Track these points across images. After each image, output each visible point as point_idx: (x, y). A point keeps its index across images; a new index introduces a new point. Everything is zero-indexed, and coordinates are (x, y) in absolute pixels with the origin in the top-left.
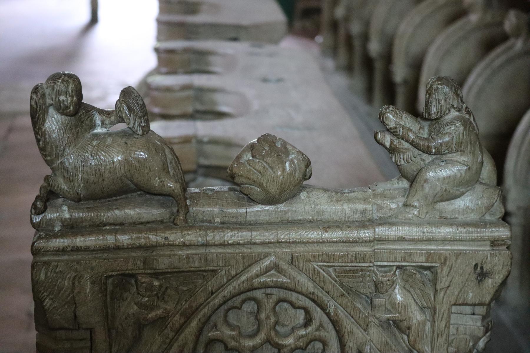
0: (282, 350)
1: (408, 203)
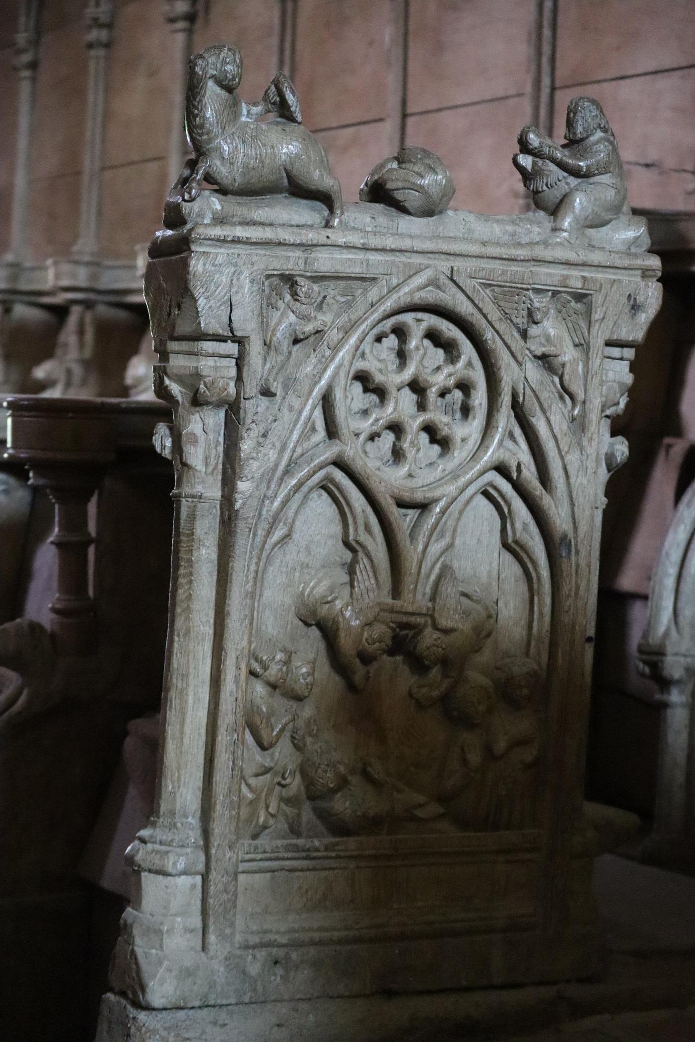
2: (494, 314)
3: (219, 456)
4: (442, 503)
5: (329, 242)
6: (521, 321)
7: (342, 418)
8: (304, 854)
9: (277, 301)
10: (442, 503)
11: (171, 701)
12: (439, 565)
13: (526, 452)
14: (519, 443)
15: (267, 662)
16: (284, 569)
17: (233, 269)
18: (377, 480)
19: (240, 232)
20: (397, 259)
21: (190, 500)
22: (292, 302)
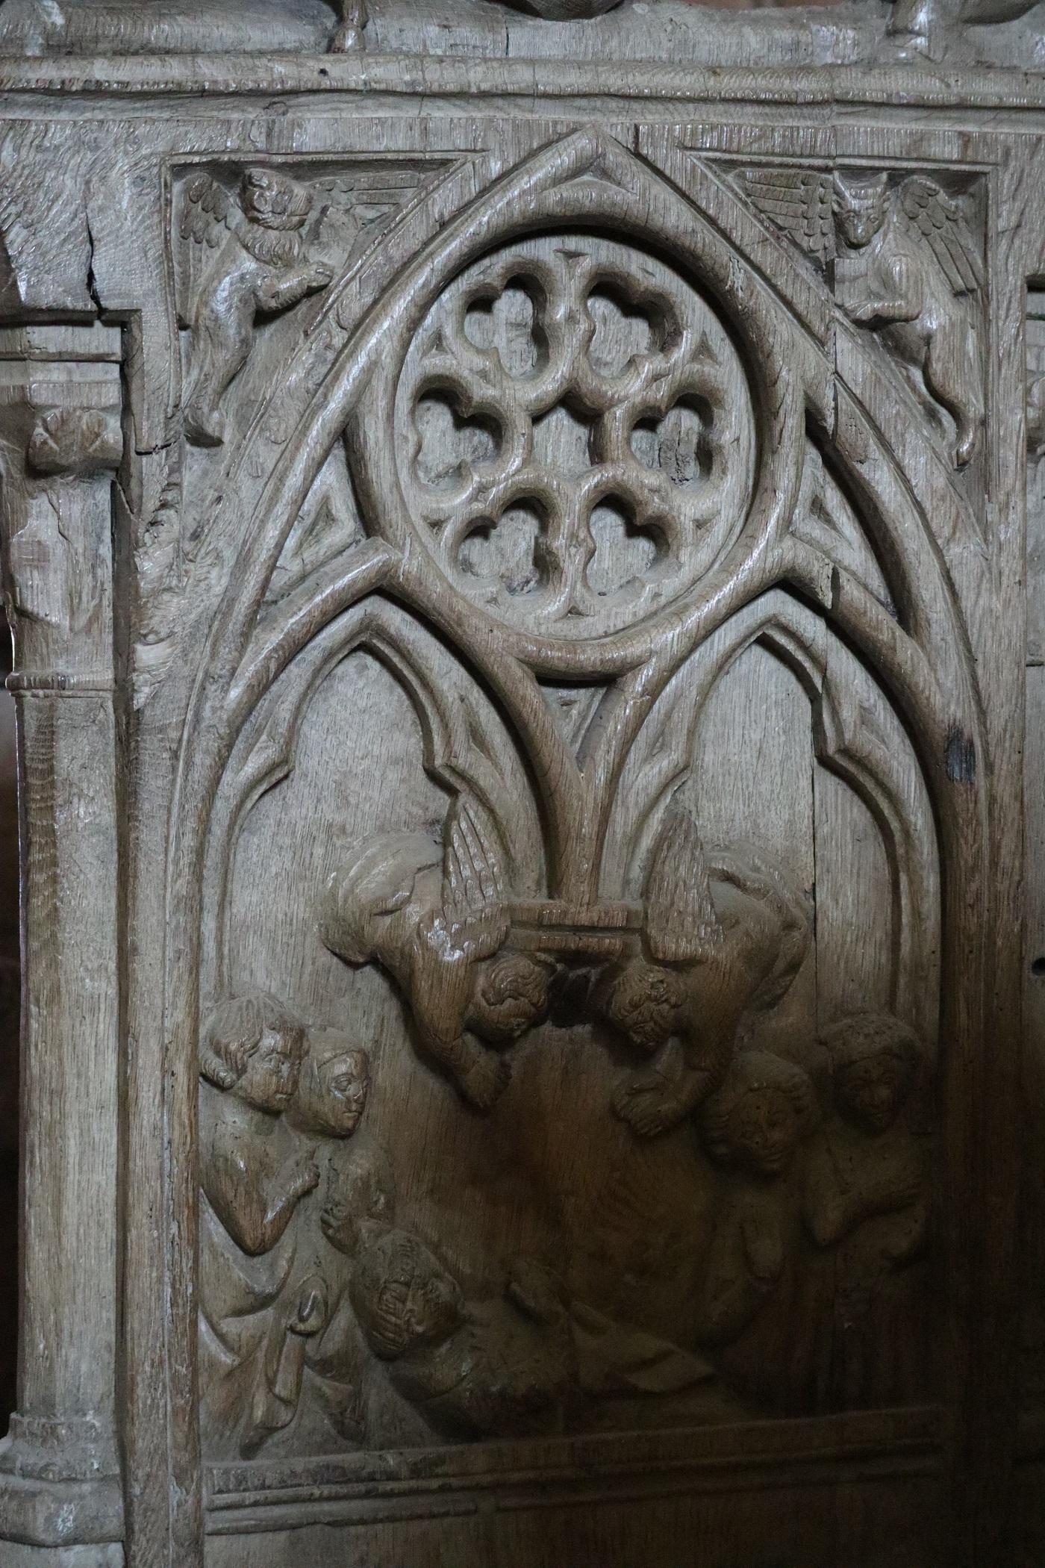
0: (607, 414)
1: (900, 25)
2: (748, 230)
3: (103, 590)
4: (647, 673)
5: (326, 83)
6: (821, 242)
7: (384, 486)
8: (362, 1487)
9: (208, 224)
10: (647, 673)
11: (32, 1152)
12: (659, 814)
13: (856, 545)
14: (839, 526)
15: (239, 1055)
16: (288, 841)
17: (90, 157)
18: (482, 625)
19: (102, 71)
20: (499, 115)
21: (41, 693)
22: (246, 227)
